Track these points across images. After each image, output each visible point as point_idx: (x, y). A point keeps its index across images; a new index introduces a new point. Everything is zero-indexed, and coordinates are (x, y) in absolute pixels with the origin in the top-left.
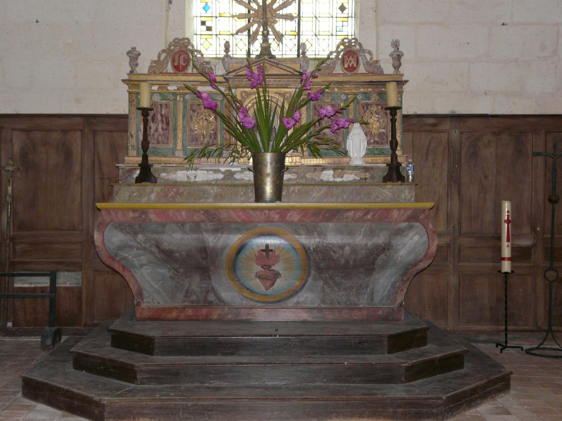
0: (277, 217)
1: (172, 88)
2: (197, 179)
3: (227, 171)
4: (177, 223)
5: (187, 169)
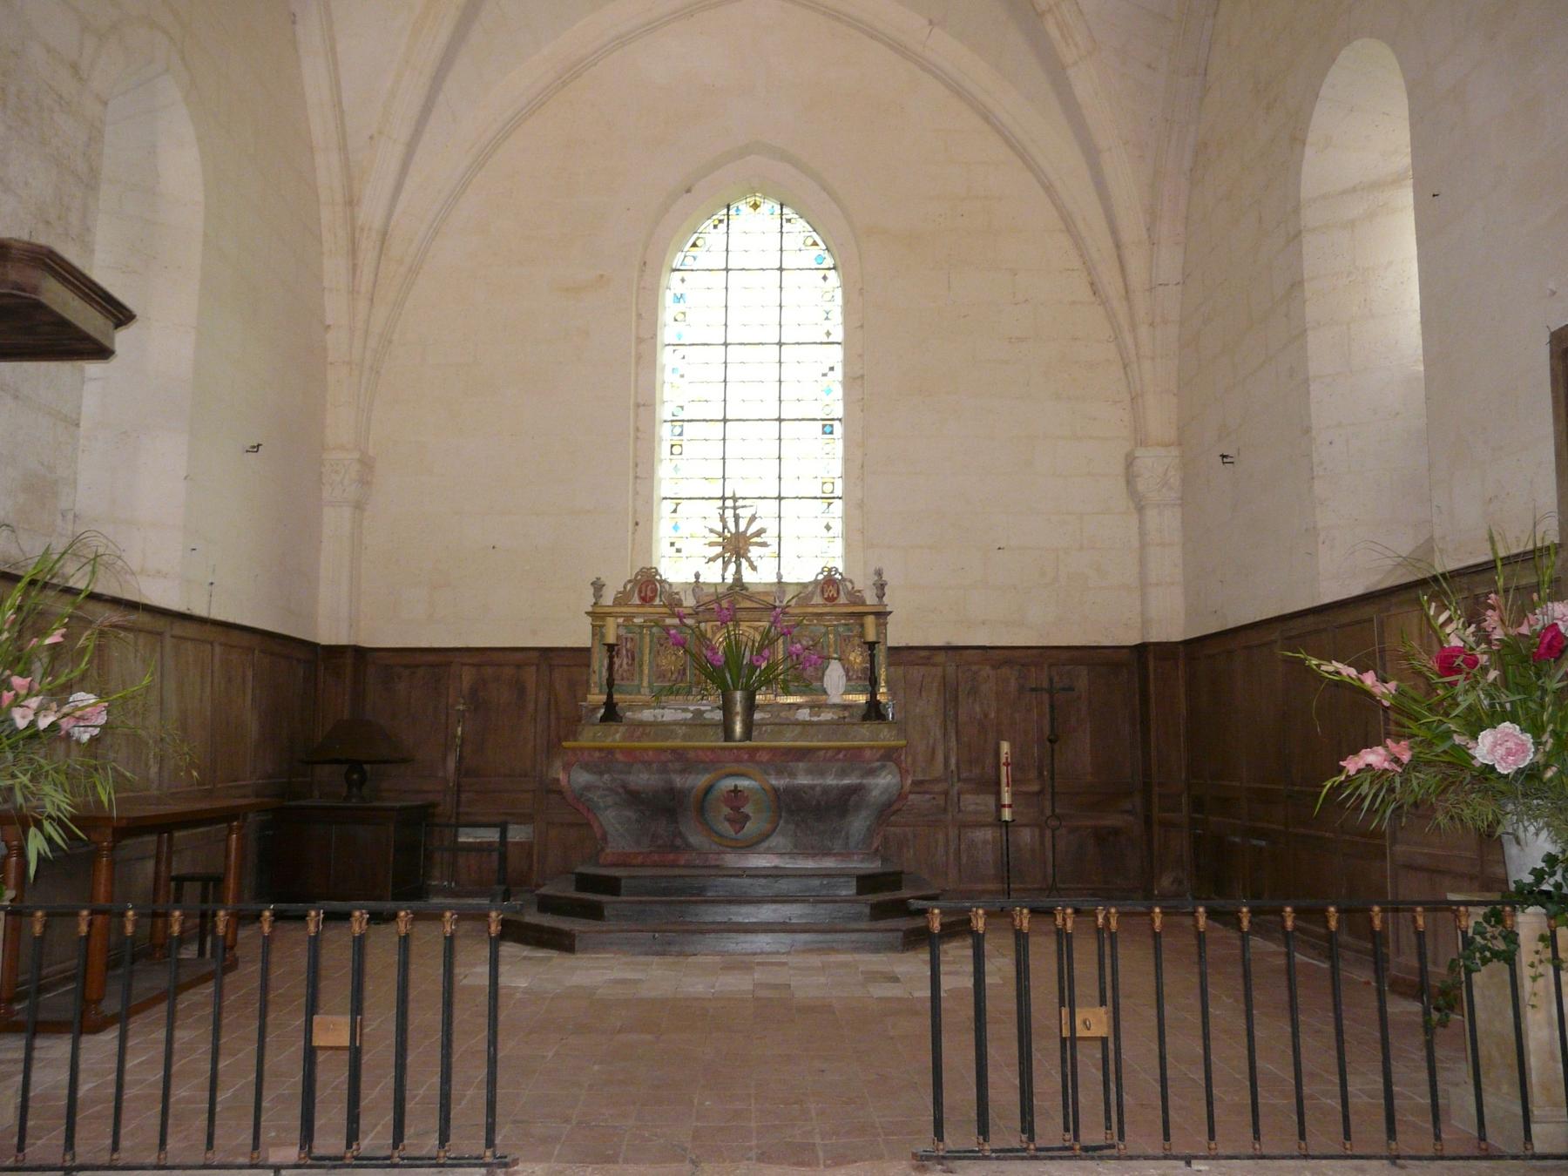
0: (746, 757)
2: (664, 719)
3: (697, 709)
4: (644, 762)
5: (654, 708)
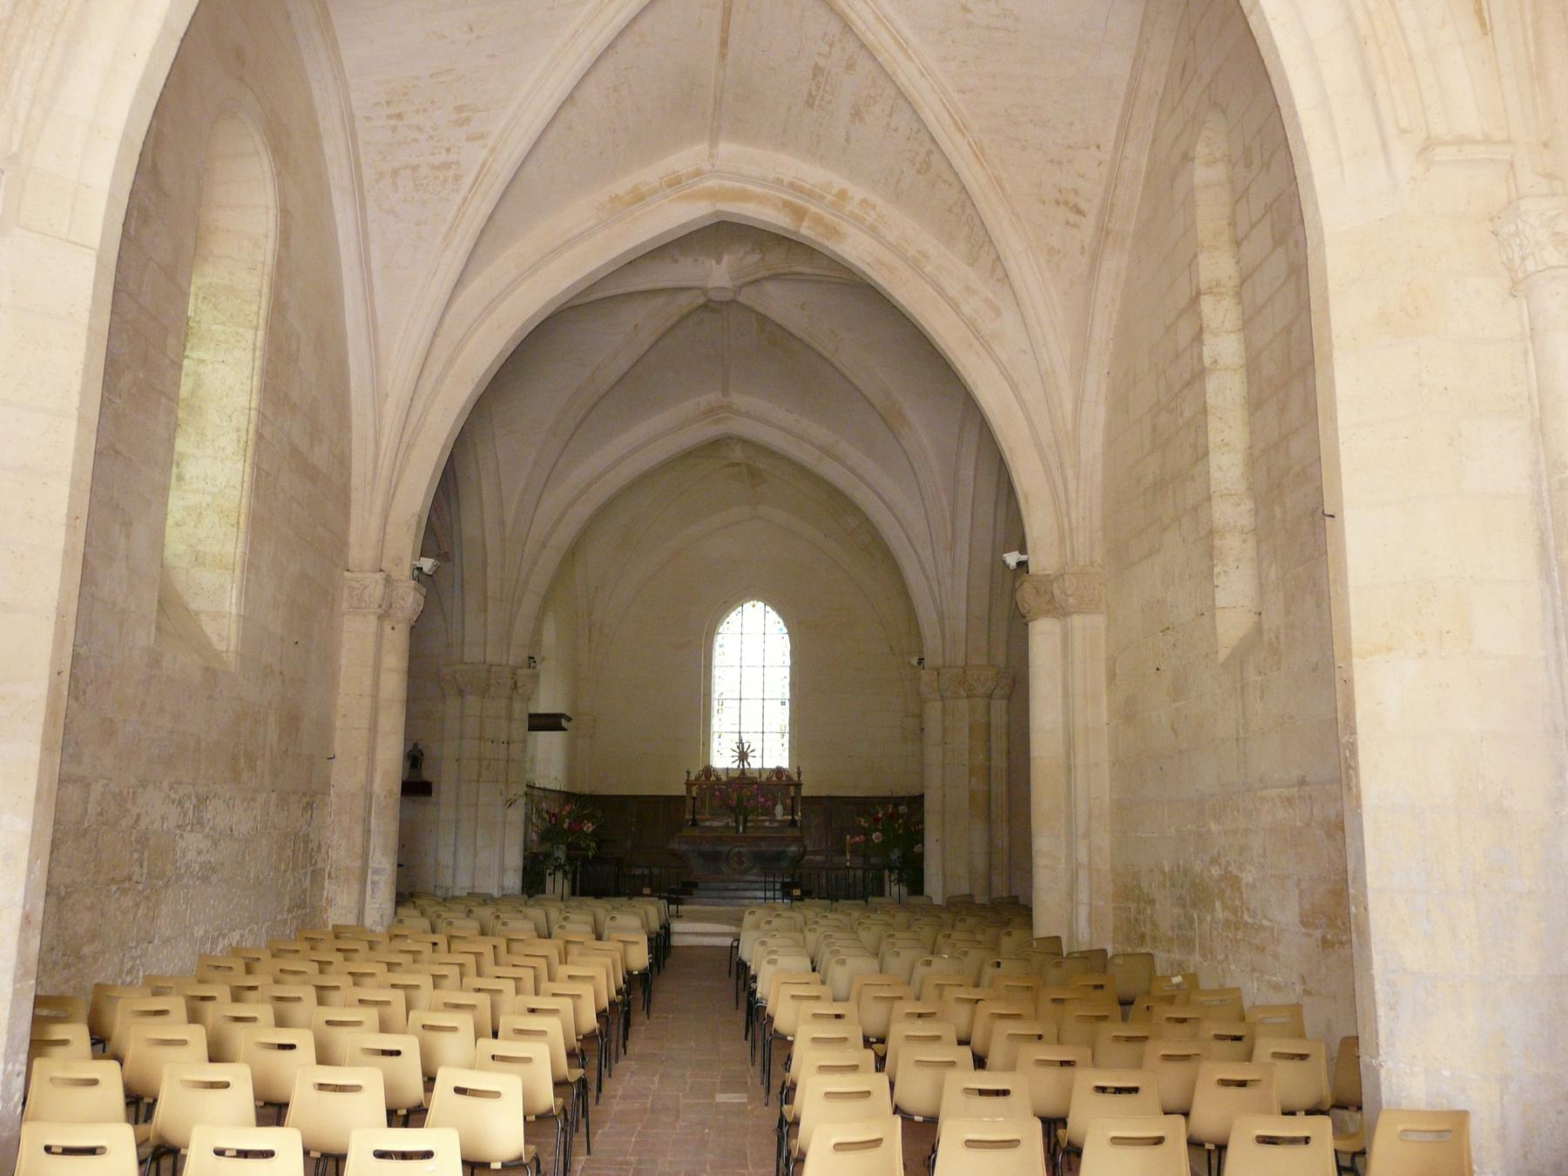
1: (704, 786)
